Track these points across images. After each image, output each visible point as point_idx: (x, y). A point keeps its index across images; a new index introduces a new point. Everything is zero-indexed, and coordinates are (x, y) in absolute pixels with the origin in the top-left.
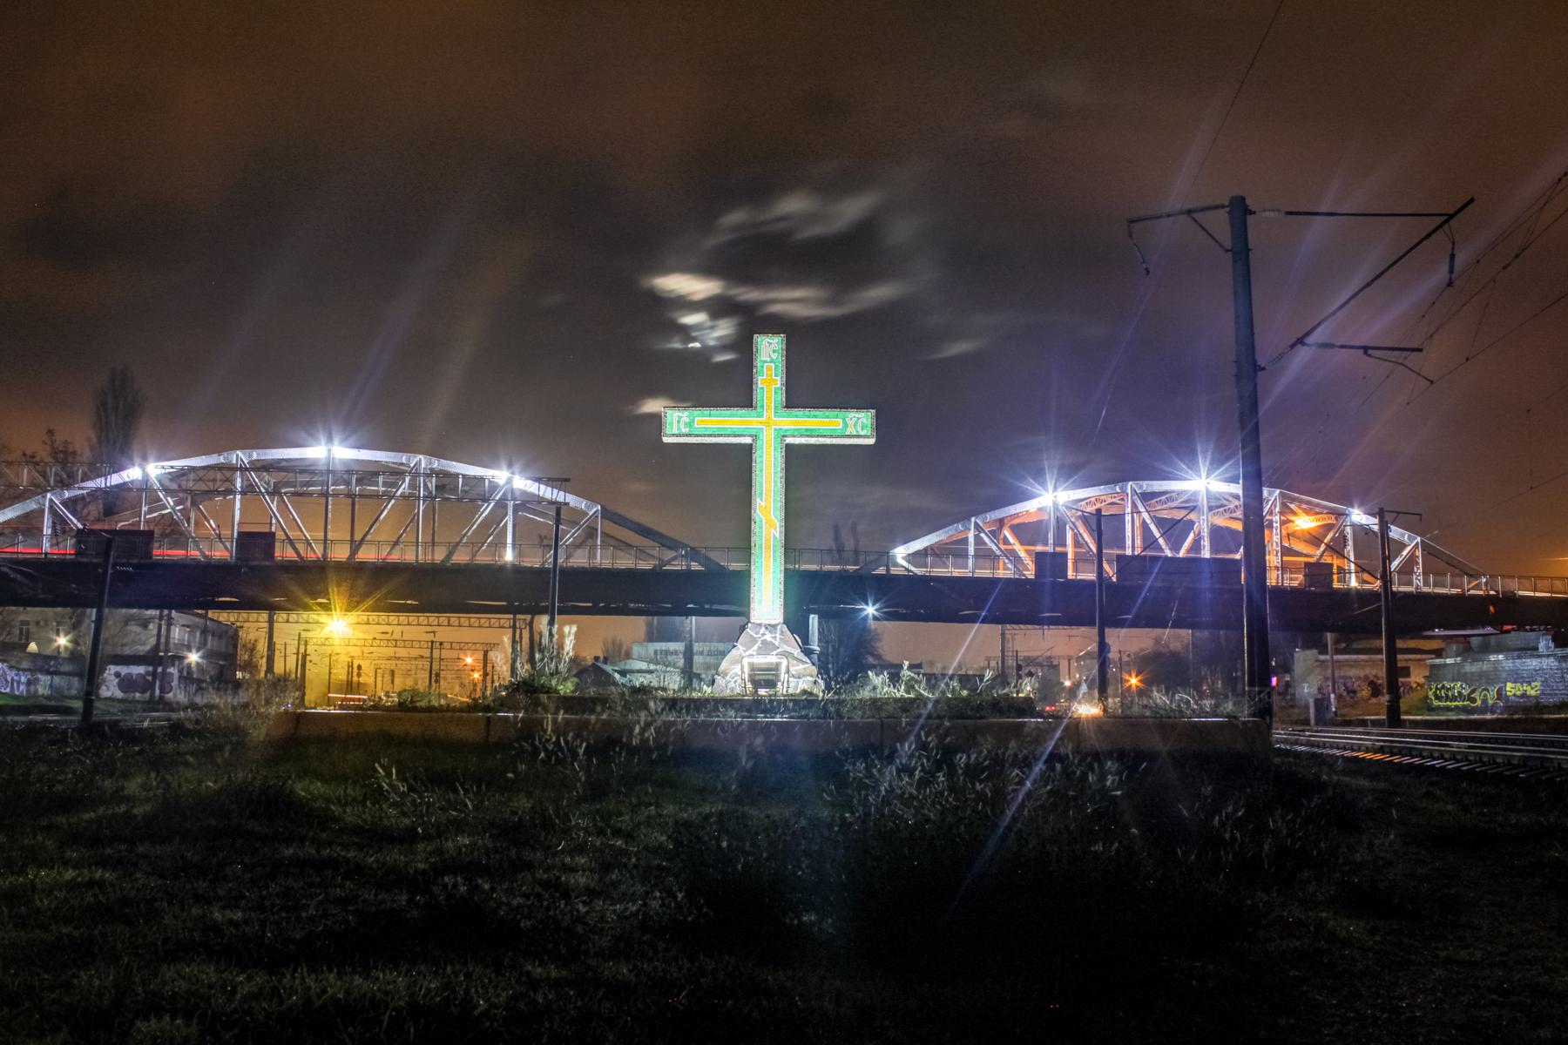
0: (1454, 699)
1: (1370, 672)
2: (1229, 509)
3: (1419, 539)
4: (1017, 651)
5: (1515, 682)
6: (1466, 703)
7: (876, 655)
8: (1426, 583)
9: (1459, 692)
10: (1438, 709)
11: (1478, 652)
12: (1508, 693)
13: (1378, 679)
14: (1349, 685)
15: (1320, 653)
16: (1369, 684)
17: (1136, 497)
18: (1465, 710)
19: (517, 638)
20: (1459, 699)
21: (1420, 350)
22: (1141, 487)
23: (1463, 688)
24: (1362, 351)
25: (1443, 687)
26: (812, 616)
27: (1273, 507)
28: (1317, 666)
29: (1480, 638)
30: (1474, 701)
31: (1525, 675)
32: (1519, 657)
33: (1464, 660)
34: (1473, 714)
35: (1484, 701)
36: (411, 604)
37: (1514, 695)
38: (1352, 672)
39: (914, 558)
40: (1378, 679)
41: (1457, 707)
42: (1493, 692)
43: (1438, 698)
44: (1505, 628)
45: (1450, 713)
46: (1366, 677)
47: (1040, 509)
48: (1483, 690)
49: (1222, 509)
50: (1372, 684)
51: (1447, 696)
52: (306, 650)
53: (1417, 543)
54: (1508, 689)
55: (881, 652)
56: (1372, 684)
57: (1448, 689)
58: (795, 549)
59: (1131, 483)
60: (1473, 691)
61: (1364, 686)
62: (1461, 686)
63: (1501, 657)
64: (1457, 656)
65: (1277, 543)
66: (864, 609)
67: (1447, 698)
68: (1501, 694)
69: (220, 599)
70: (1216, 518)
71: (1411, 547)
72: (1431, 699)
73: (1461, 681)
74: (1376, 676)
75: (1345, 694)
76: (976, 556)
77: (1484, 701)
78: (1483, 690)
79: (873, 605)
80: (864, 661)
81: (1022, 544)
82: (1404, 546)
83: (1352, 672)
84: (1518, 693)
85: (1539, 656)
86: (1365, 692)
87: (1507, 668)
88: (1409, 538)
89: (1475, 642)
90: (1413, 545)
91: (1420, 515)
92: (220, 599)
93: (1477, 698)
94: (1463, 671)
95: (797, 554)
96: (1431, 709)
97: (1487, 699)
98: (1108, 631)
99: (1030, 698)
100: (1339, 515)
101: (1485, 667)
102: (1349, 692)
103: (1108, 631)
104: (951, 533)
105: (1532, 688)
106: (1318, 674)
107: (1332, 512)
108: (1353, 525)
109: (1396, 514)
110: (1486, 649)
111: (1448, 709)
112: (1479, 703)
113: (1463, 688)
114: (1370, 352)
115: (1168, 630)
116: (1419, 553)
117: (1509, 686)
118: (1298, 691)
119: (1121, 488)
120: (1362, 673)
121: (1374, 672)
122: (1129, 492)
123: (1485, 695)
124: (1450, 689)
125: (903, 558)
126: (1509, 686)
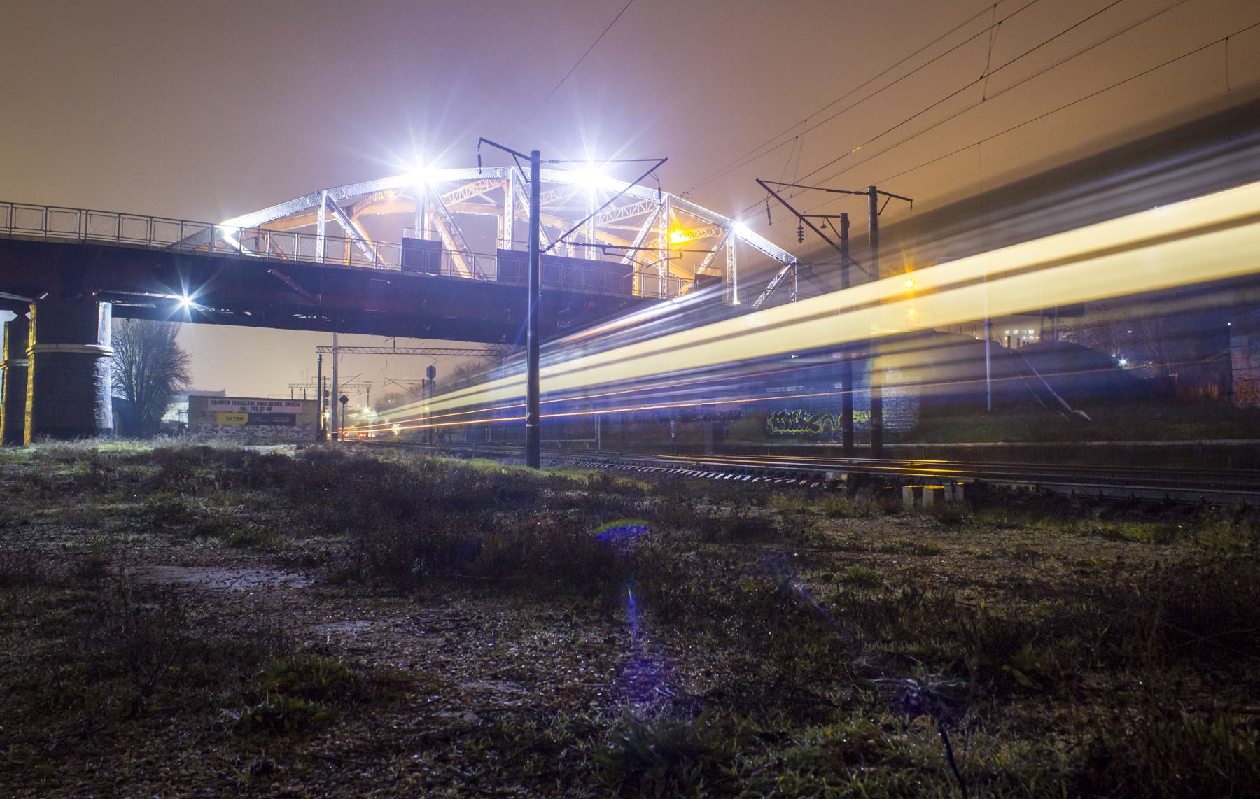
0: (795, 426)
7: (184, 378)
10: (778, 436)
18: (807, 437)
19: (434, 352)
25: (783, 415)
26: (102, 304)
30: (816, 428)
34: (816, 441)
35: (827, 429)
36: (1082, 416)
37: (859, 422)
39: (243, 235)
41: (797, 434)
43: (777, 425)
45: (791, 441)
48: (826, 418)
51: (787, 423)
55: (189, 375)
57: (788, 417)
58: (80, 210)
60: (815, 419)
62: (803, 413)
66: (174, 301)
67: (787, 426)
69: (1087, 417)
72: (770, 427)
77: (827, 429)
79: (191, 292)
80: (170, 384)
91: (911, 201)
92: (1087, 417)
95: (84, 216)
96: (770, 436)
97: (829, 427)
99: (435, 466)
100: (720, 226)
108: (737, 241)
109: (888, 197)
111: (789, 436)
112: (821, 430)
115: (514, 346)
119: (503, 173)
122: (511, 177)
123: (829, 423)
124: (790, 416)
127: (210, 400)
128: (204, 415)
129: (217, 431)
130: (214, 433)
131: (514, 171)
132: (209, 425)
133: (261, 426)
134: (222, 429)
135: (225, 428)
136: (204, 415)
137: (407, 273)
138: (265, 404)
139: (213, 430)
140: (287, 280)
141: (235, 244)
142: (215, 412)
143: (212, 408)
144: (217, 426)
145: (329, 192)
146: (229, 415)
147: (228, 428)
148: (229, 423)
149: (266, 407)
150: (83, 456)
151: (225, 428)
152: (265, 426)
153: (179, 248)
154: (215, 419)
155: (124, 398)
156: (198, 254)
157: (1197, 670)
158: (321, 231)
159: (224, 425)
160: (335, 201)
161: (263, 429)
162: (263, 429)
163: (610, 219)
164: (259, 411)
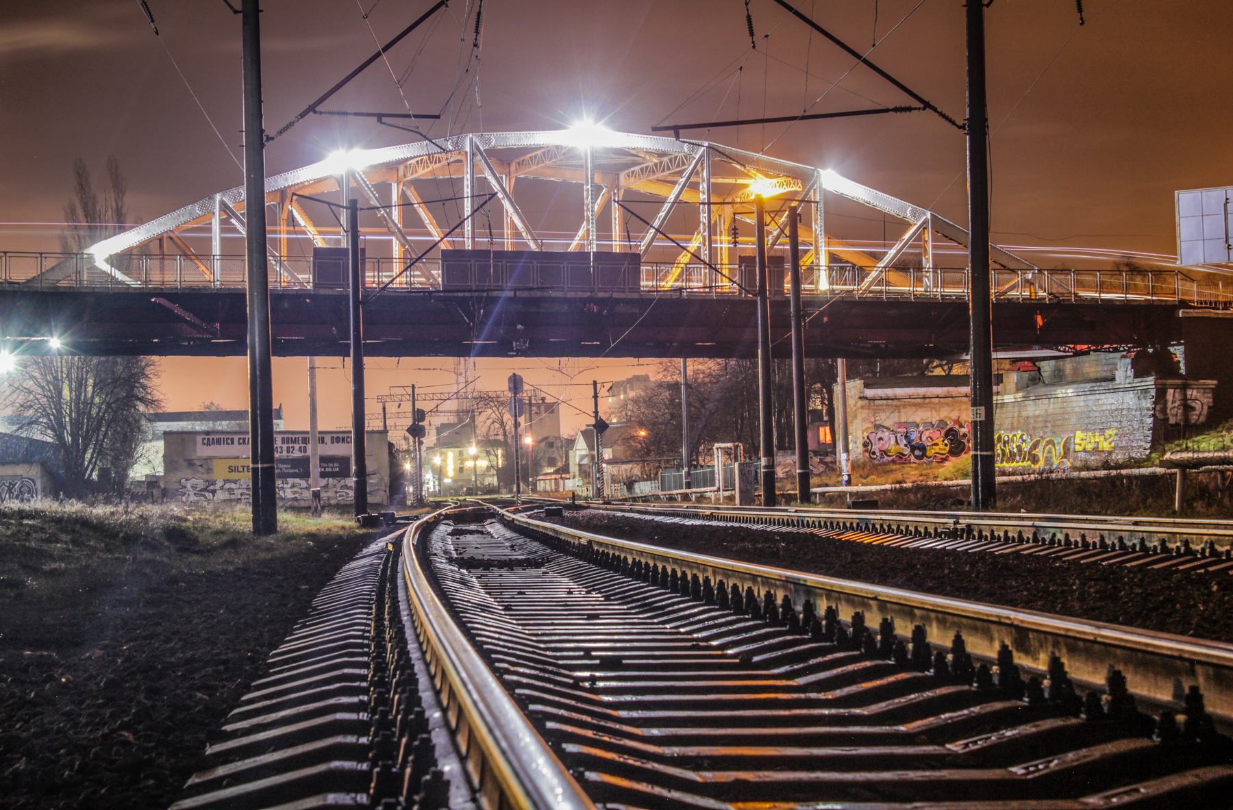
1: (948, 414)
2: (647, 167)
3: (929, 215)
4: (413, 387)
5: (1086, 430)
6: (1025, 464)
8: (936, 286)
9: (1019, 447)
11: (1052, 385)
12: (1078, 448)
13: (961, 426)
14: (914, 436)
15: (867, 386)
16: (947, 435)
17: (479, 157)
20: (1017, 458)
21: (438, 117)
22: (488, 141)
23: (1024, 441)
24: (376, 118)
27: (698, 167)
28: (862, 407)
29: (1052, 362)
31: (1098, 420)
32: (1092, 392)
33: (1026, 398)
38: (919, 416)
39: (122, 260)
40: (961, 426)
42: (1060, 441)
44: (1079, 347)
46: (942, 422)
47: (318, 181)
49: (637, 168)
50: (951, 434)
52: (895, 470)
53: (925, 222)
54: (1077, 441)
56: (951, 434)
57: (1005, 443)
59: (471, 135)
60: (1035, 446)
61: (939, 438)
63: (1070, 391)
64: (1018, 390)
65: (704, 224)
68: (1069, 449)
70: (632, 180)
71: (917, 226)
73: (1023, 431)
74: (957, 422)
75: (907, 451)
76: (224, 256)
78: (1048, 443)
81: (315, 225)
82: (906, 225)
83: (919, 416)
84: (1089, 447)
85: (1115, 391)
86: (942, 447)
87: (1077, 409)
88: (914, 214)
89: (1047, 368)
90: (919, 223)
93: (1040, 455)
94: (1024, 414)
98: (367, 361)
100: (804, 178)
101: (1051, 409)
102: (913, 449)
103: (367, 361)
104: (182, 219)
105: (1106, 439)
106: (864, 420)
107: (794, 175)
110: (1059, 378)
113: (1024, 441)
114: (384, 119)
116: (928, 236)
117: (1079, 434)
118: (523, 443)
119: (456, 145)
120: (934, 418)
121: (954, 415)
125: (107, 261)
126: (1079, 434)
127: (199, 439)
128: (191, 464)
129: (214, 492)
130: (210, 496)
131: (471, 140)
132: (200, 483)
133: (290, 481)
134: (222, 488)
135: (227, 486)
136: (191, 464)
137: (322, 292)
138: (294, 441)
139: (205, 490)
140: (177, 310)
141: (106, 268)
142: (211, 458)
143: (202, 451)
144: (214, 483)
145: (224, 195)
146: (233, 463)
147: (233, 486)
148: (235, 476)
149: (297, 446)
150: (1059, 351)
151: (227, 486)
152: (297, 480)
153: (39, 285)
154: (209, 470)
155: (50, 440)
156: (62, 290)
157: (152, 638)
158: (216, 249)
159: (226, 481)
160: (231, 206)
161: (293, 486)
162: (293, 486)
163: (669, 169)
164: (285, 453)
